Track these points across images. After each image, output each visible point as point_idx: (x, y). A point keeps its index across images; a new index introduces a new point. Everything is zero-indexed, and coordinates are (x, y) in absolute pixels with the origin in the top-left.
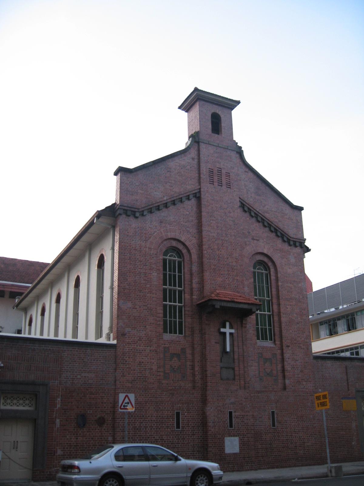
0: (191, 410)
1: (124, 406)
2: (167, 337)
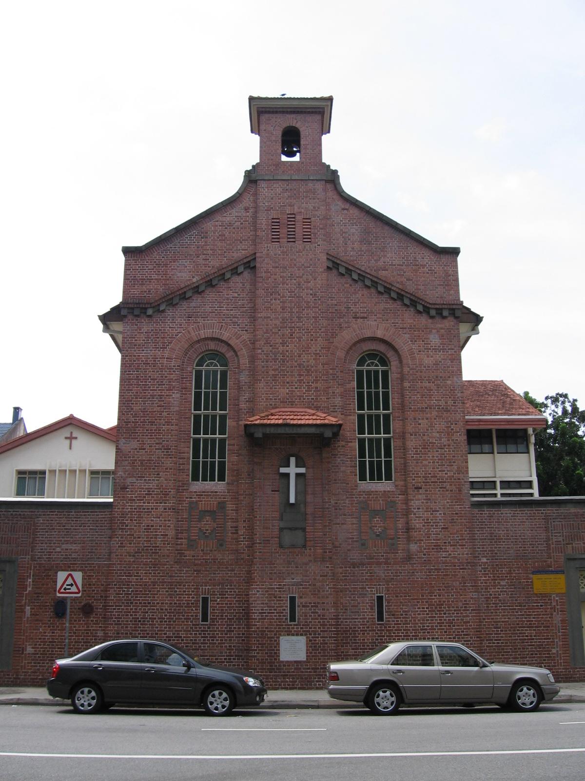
0: (229, 595)
1: (65, 589)
2: (199, 486)
